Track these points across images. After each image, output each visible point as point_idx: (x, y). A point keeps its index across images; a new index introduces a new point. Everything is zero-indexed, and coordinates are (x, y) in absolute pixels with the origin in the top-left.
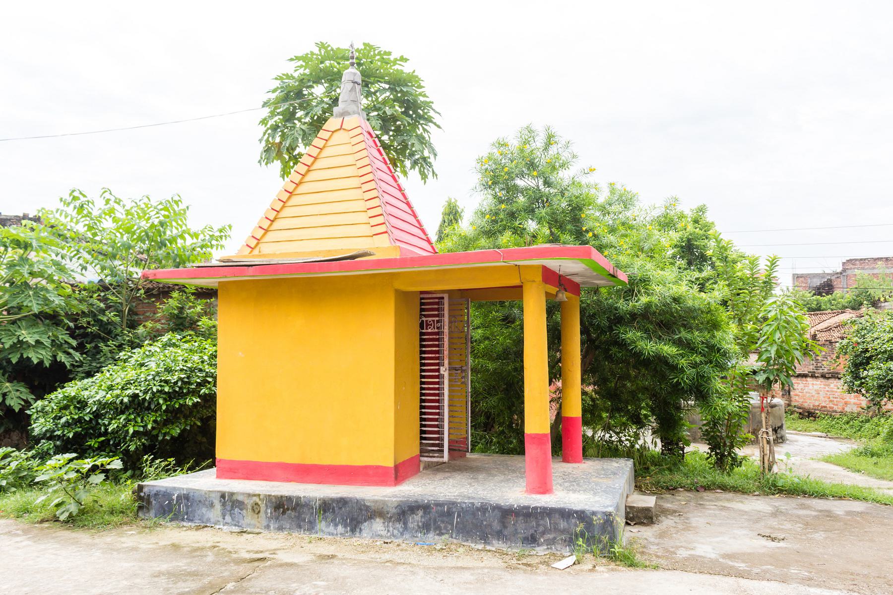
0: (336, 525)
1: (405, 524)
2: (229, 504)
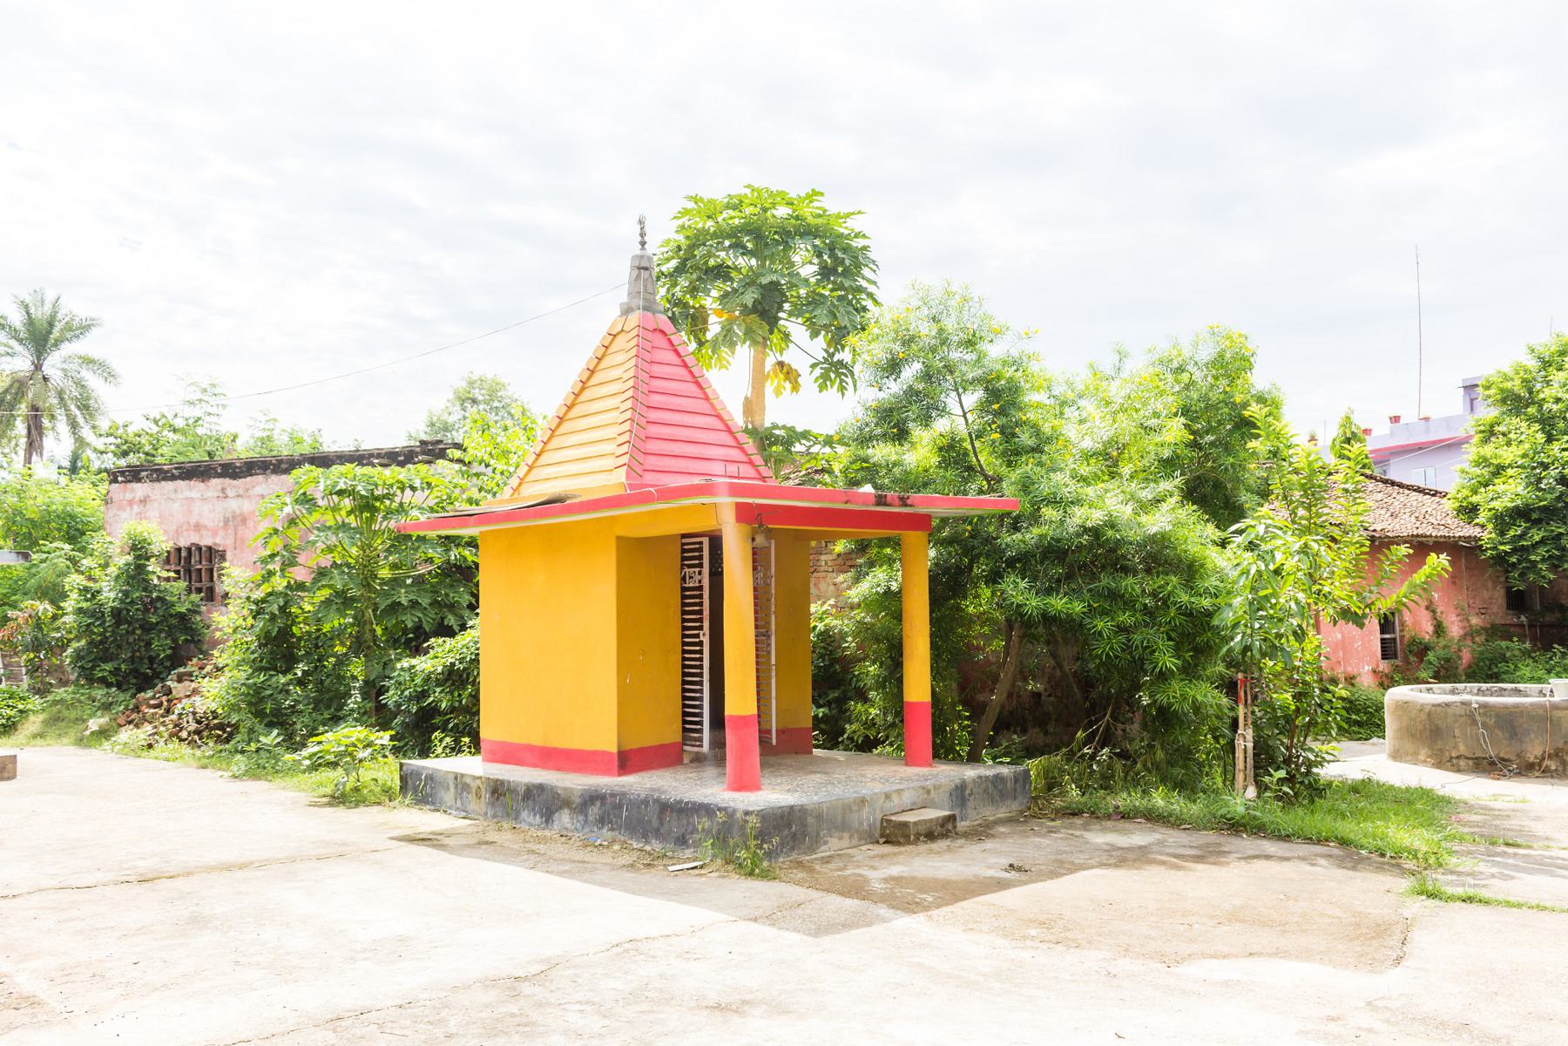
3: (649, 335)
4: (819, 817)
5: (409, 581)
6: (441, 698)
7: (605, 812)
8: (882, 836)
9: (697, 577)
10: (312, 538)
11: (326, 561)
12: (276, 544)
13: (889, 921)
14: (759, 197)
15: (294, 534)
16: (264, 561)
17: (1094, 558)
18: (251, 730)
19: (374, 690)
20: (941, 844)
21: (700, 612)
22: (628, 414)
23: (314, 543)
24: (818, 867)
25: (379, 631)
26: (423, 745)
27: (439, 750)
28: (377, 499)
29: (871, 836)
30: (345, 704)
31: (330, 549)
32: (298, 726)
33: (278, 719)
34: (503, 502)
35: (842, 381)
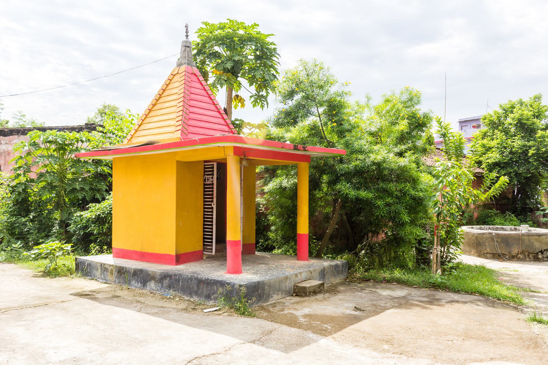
0: (138, 283)
1: (162, 284)
2: (103, 269)
3: (190, 75)
4: (270, 286)
5: (80, 180)
6: (94, 229)
7: (171, 282)
8: (294, 292)
9: (211, 180)
10: (37, 160)
11: (44, 170)
12: (21, 163)
13: (316, 342)
14: (233, 25)
15: (30, 160)
16: (16, 170)
17: (375, 176)
18: (9, 241)
19: (64, 224)
20: (320, 296)
21: (212, 195)
22: (181, 108)
23: (38, 162)
24: (271, 309)
25: (67, 200)
26: (86, 248)
27: (93, 252)
28: (66, 145)
29: (290, 293)
30: (51, 230)
31: (46, 166)
32: (30, 239)
33: (22, 237)
34: (125, 144)
35: (262, 103)
